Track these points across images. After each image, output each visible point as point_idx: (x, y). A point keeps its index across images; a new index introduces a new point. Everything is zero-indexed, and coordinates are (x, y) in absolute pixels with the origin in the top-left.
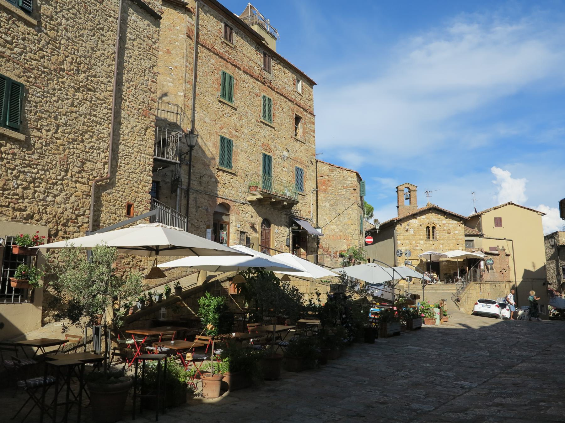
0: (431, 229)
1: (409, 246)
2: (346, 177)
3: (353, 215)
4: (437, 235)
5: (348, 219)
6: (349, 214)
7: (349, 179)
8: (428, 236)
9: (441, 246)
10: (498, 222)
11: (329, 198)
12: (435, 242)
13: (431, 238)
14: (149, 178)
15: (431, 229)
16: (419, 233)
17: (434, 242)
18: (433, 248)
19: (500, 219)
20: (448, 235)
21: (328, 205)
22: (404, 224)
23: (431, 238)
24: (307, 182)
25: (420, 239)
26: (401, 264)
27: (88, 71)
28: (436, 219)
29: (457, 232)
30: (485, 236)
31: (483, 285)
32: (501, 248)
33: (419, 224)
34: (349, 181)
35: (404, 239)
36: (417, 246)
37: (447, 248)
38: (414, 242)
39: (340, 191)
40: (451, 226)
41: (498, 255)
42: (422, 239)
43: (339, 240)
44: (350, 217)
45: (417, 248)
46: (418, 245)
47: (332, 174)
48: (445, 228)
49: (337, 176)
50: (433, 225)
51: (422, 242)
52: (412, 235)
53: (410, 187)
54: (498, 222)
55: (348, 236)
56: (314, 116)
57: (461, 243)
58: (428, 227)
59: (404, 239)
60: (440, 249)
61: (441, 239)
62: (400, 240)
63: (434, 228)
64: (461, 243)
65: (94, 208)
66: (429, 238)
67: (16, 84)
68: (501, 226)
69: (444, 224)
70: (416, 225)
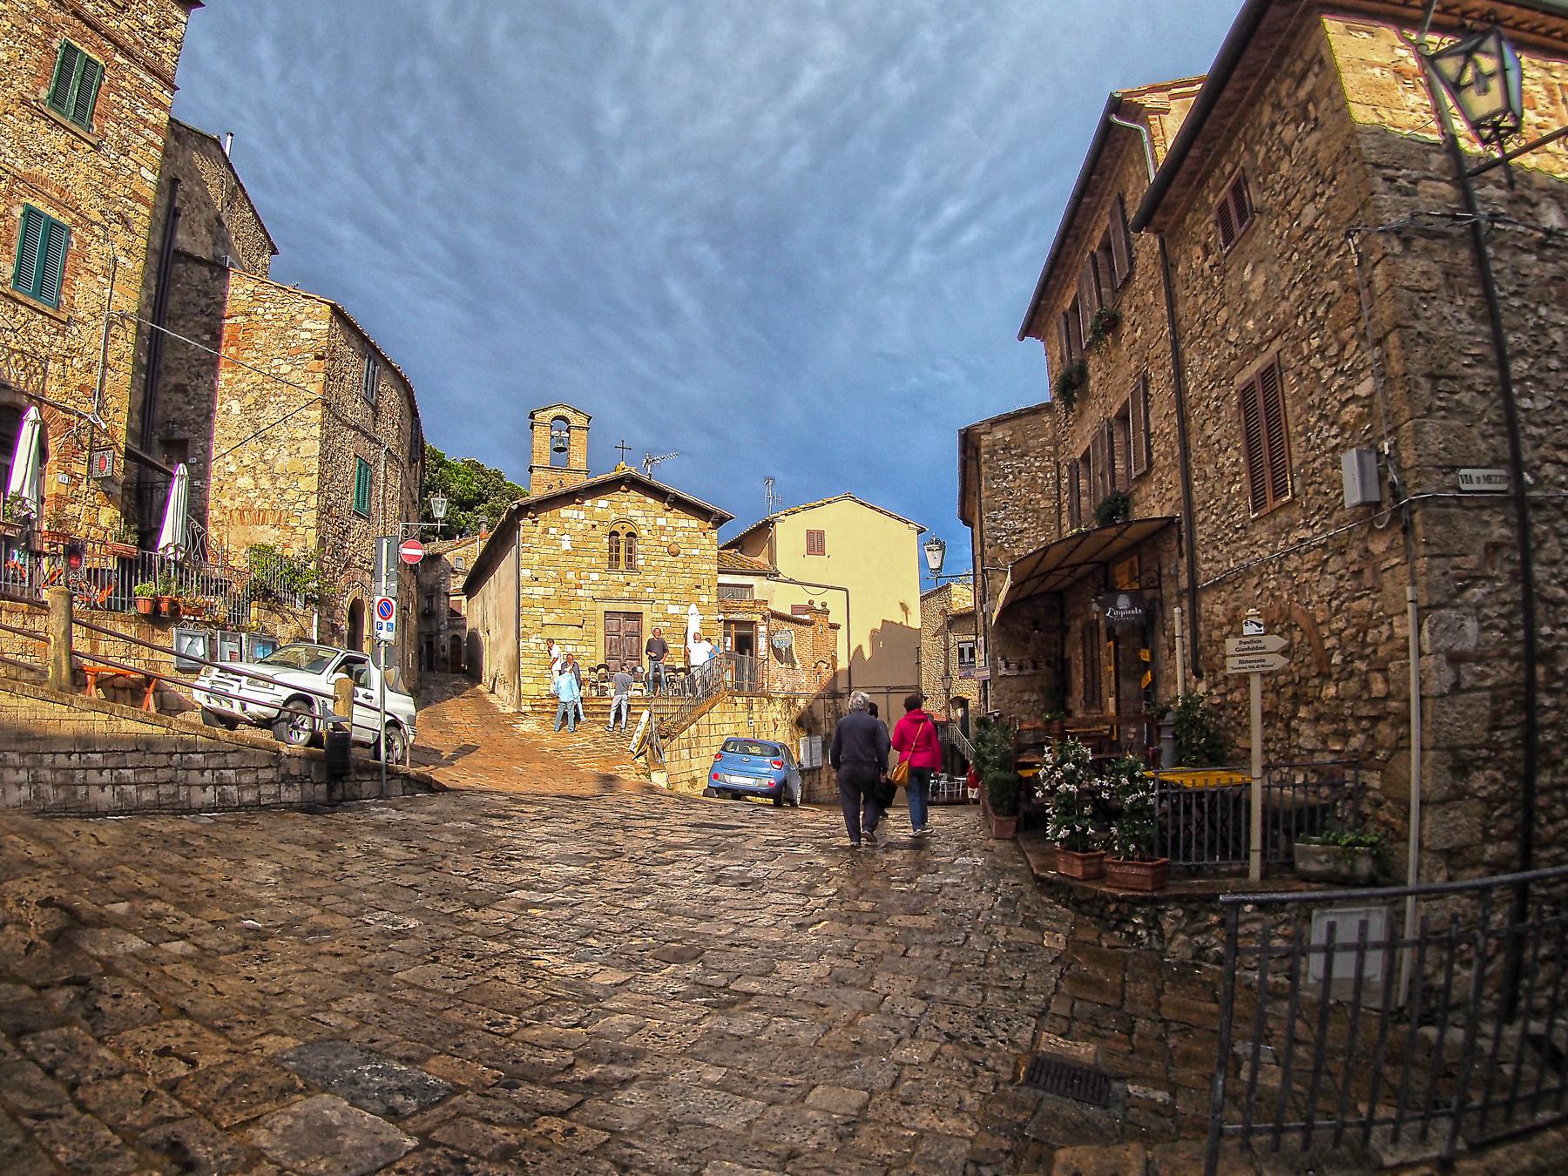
2: (299, 317)
7: (307, 324)
8: (614, 560)
10: (816, 542)
13: (622, 567)
15: (622, 537)
17: (629, 578)
19: (821, 534)
21: (236, 407)
22: (545, 517)
23: (622, 567)
24: (87, 277)
28: (640, 513)
30: (781, 577)
31: (761, 703)
32: (820, 607)
34: (306, 330)
36: (579, 587)
38: (571, 576)
39: (276, 362)
41: (812, 623)
42: (592, 568)
43: (260, 528)
45: (580, 592)
47: (260, 311)
52: (567, 553)
53: (569, 414)
54: (816, 542)
55: (284, 515)
56: (176, 89)
61: (650, 568)
68: (809, 533)
69: (662, 528)
70: (581, 526)
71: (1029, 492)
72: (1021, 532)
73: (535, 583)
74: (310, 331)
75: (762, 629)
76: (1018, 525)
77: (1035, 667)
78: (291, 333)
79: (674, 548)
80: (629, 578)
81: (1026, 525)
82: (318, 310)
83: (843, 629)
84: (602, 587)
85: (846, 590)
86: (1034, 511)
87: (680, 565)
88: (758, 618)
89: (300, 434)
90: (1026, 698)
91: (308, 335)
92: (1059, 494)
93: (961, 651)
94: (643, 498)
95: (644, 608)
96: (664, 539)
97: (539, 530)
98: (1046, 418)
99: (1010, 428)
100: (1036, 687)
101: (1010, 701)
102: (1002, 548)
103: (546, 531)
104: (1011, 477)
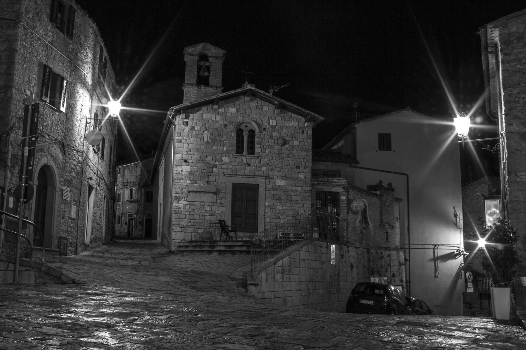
8: (239, 150)
9: (264, 169)
12: (253, 161)
13: (245, 152)
16: (220, 141)
19: (389, 136)
25: (222, 152)
27: (436, 248)
42: (227, 153)
45: (215, 170)
46: (217, 163)
48: (275, 134)
51: (226, 159)
57: (304, 164)
61: (264, 154)
62: (179, 152)
64: (304, 164)
65: (409, 313)
66: (241, 152)
67: (111, 155)
69: (273, 128)
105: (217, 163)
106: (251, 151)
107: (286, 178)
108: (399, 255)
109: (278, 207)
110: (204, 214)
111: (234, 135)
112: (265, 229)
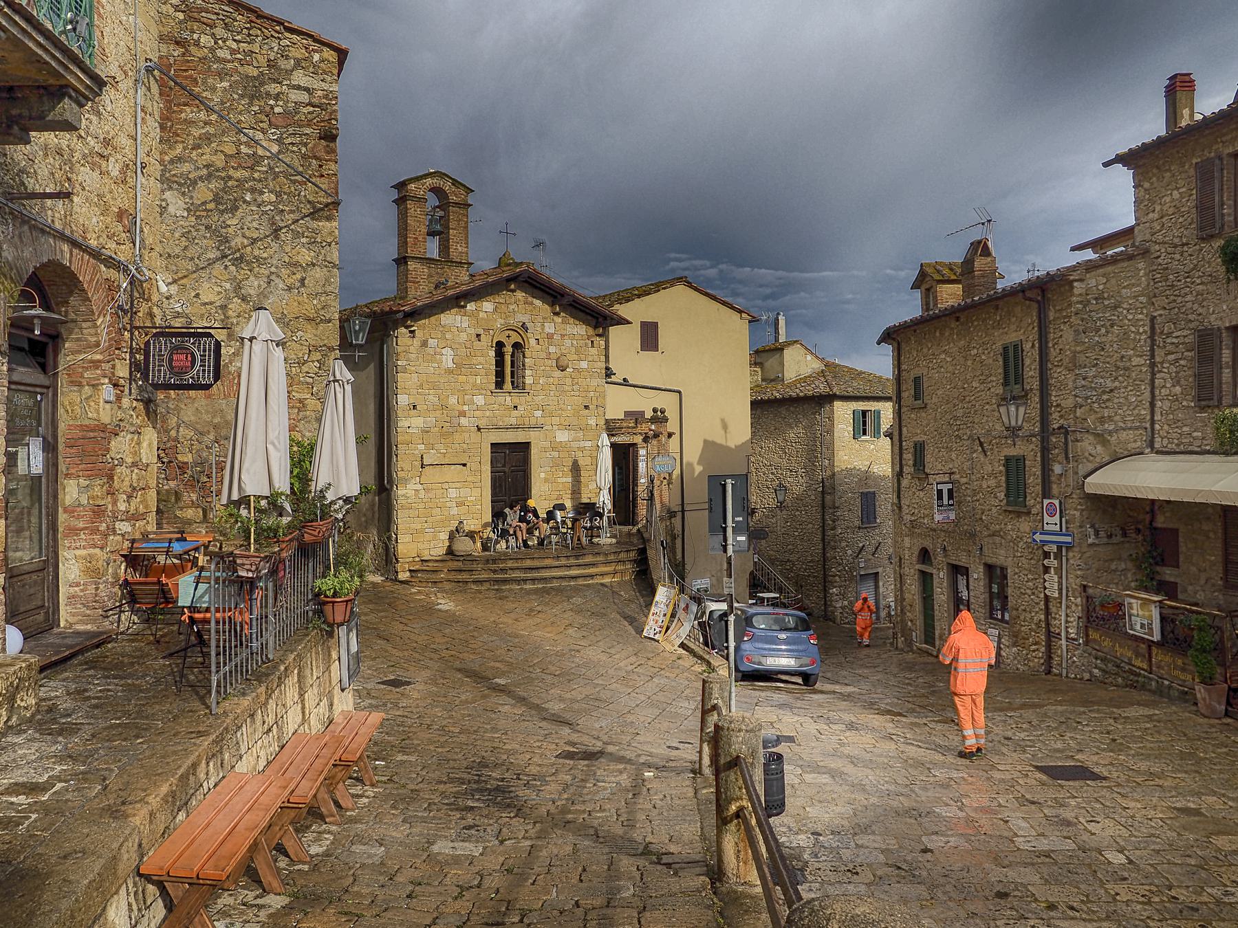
0: (508, 350)
1: (438, 413)
3: (318, 273)
4: (528, 372)
5: (290, 289)
6: (296, 264)
7: (299, 78)
8: (499, 384)
9: (538, 413)
10: (650, 337)
11: (186, 167)
13: (508, 386)
14: (702, 878)
15: (508, 350)
17: (516, 401)
18: (513, 421)
20: (558, 373)
22: (422, 327)
26: (406, 481)
29: (584, 365)
33: (472, 331)
34: (299, 87)
35: (421, 386)
36: (463, 414)
37: (556, 420)
38: (453, 400)
40: (568, 342)
42: (479, 389)
44: (303, 280)
45: (464, 421)
46: (466, 408)
47: (206, 40)
48: (552, 349)
49: (233, 52)
50: (516, 338)
51: (480, 400)
52: (449, 371)
58: (500, 345)
59: (421, 386)
60: (533, 421)
63: (517, 346)
64: (595, 402)
68: (655, 348)
69: (550, 336)
71: (1121, 347)
72: (1112, 391)
73: (413, 412)
74: (307, 90)
75: (642, 452)
76: (1110, 384)
77: (1125, 535)
78: (273, 88)
79: (563, 362)
80: (516, 401)
81: (1117, 384)
82: (316, 57)
83: (676, 438)
84: (488, 413)
85: (679, 392)
86: (1126, 369)
87: (569, 381)
88: (638, 439)
89: (305, 256)
90: (1113, 567)
91: (304, 97)
92: (1152, 350)
93: (940, 492)
94: (530, 299)
95: (532, 437)
96: (552, 349)
97: (417, 342)
98: (1141, 265)
99: (1104, 275)
100: (1125, 555)
101: (1098, 570)
102: (1091, 409)
103: (424, 344)
104: (1103, 330)
105: (466, 408)
106: (518, 385)
107: (568, 427)
108: (611, 754)
109: (559, 480)
110: (448, 504)
111: (492, 353)
112: (450, 551)
